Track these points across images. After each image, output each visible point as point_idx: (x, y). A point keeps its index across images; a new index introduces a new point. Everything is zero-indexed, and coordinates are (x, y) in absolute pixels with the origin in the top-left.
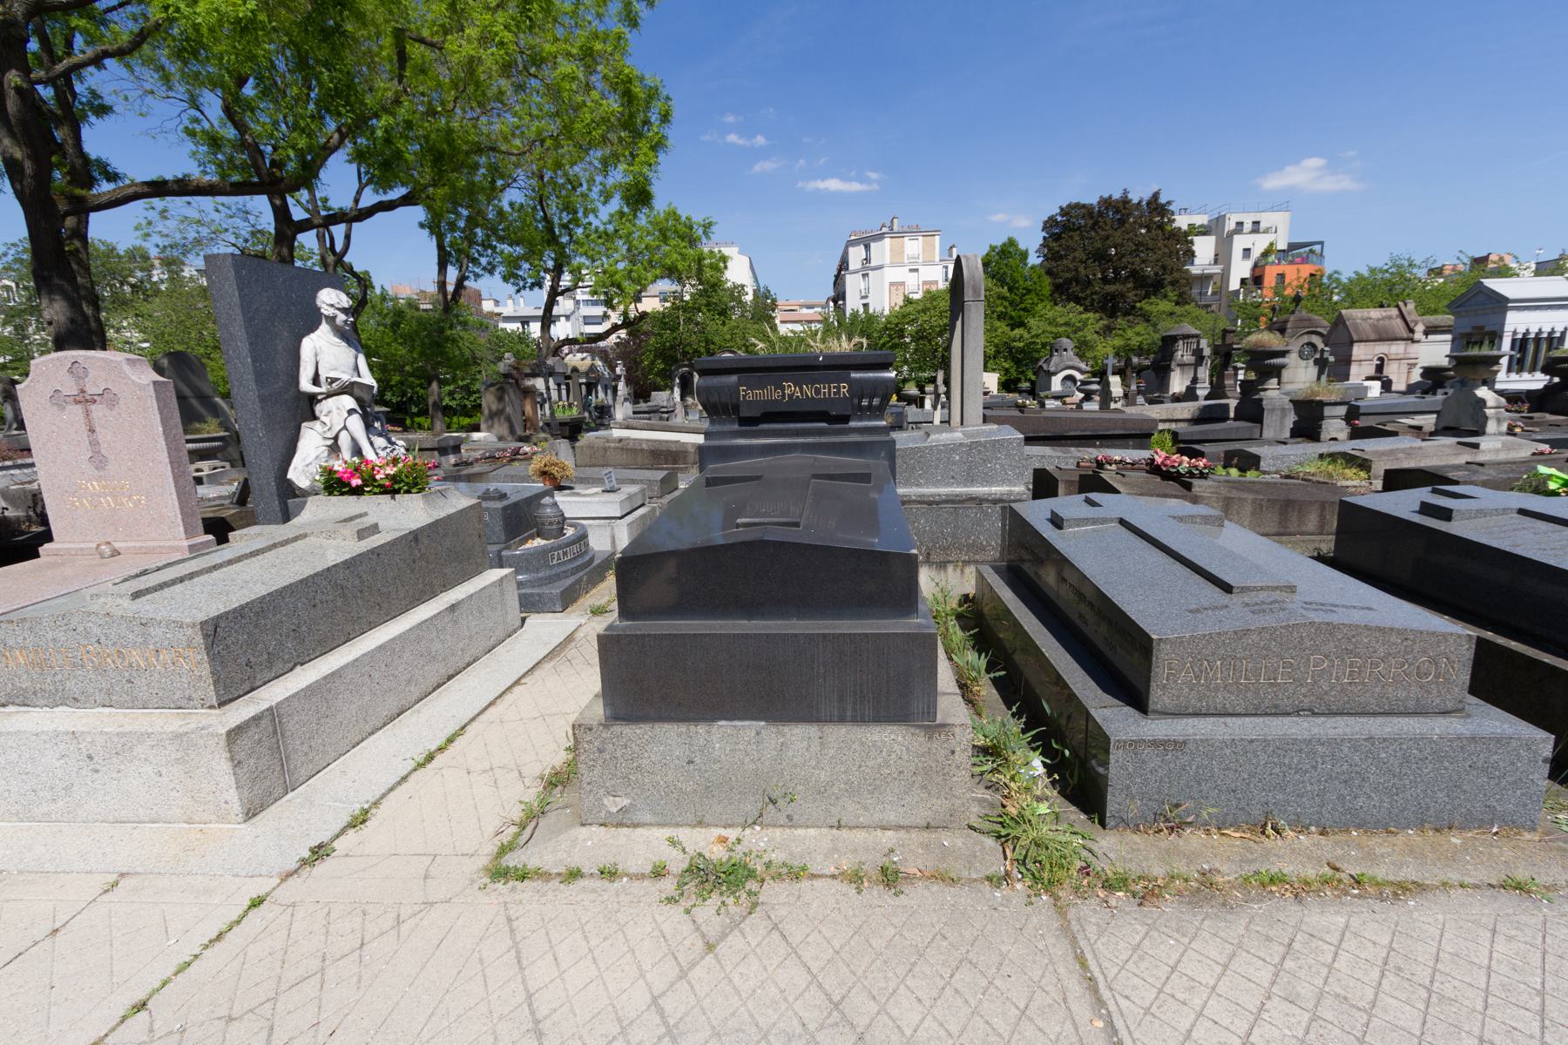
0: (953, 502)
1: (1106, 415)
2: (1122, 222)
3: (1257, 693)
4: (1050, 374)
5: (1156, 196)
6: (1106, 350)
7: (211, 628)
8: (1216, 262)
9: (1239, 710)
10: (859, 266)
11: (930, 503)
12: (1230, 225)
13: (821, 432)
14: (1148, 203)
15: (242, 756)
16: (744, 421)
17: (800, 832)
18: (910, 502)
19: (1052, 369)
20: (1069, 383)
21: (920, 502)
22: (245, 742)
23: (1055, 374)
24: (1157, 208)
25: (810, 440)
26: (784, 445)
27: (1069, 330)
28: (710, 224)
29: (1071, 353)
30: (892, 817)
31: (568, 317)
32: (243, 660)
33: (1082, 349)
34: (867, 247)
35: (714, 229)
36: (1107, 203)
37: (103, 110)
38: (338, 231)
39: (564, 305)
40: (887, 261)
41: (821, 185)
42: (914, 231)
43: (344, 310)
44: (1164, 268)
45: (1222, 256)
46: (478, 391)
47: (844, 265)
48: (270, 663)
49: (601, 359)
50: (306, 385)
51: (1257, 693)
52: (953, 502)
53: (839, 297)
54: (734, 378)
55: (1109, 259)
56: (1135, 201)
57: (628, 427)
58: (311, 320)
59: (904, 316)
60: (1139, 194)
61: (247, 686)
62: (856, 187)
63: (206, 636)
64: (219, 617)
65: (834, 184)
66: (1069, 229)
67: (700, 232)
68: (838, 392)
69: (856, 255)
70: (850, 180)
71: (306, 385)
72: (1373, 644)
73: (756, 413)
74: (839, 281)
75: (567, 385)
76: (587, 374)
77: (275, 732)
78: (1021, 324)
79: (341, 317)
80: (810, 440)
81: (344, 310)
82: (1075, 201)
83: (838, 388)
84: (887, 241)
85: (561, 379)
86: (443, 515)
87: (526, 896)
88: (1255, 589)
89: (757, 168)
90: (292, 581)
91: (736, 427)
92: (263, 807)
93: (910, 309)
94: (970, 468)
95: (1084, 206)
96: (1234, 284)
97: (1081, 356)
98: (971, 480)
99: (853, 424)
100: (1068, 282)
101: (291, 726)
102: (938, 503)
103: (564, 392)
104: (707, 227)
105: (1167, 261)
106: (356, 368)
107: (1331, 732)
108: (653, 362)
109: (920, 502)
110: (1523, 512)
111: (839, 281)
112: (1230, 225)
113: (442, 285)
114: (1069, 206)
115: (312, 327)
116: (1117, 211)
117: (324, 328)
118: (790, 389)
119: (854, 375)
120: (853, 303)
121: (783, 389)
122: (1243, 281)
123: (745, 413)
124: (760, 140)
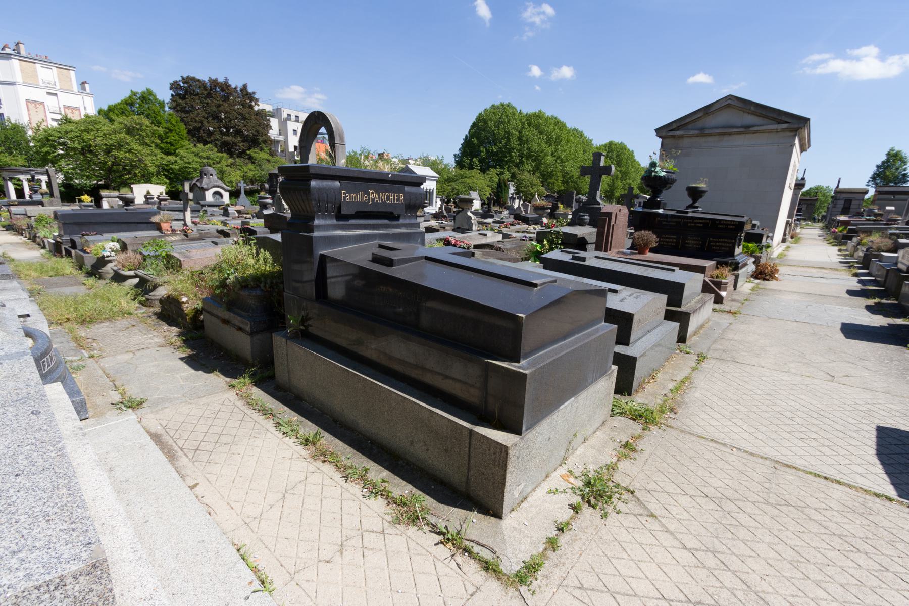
1: (98, 211)
2: (226, 99)
4: (203, 190)
5: (245, 86)
6: (235, 176)
8: (280, 134)
12: (284, 115)
14: (242, 90)
16: (340, 216)
19: (205, 187)
20: (218, 197)
23: (207, 190)
24: (247, 96)
25: (381, 231)
27: (211, 162)
29: (215, 177)
33: (222, 174)
36: (214, 83)
42: (46, 61)
44: (257, 131)
45: (283, 131)
46: (135, 175)
54: (337, 183)
55: (221, 120)
56: (233, 86)
60: (236, 83)
66: (188, 92)
73: (352, 211)
78: (173, 153)
80: (381, 231)
82: (192, 75)
91: (334, 222)
93: (69, 127)
95: (199, 81)
96: (291, 149)
97: (221, 179)
99: (402, 221)
100: (195, 128)
105: (260, 129)
110: (596, 257)
112: (284, 115)
114: (188, 77)
116: (222, 90)
119: (407, 189)
121: (368, 194)
122: (295, 148)
123: (344, 211)
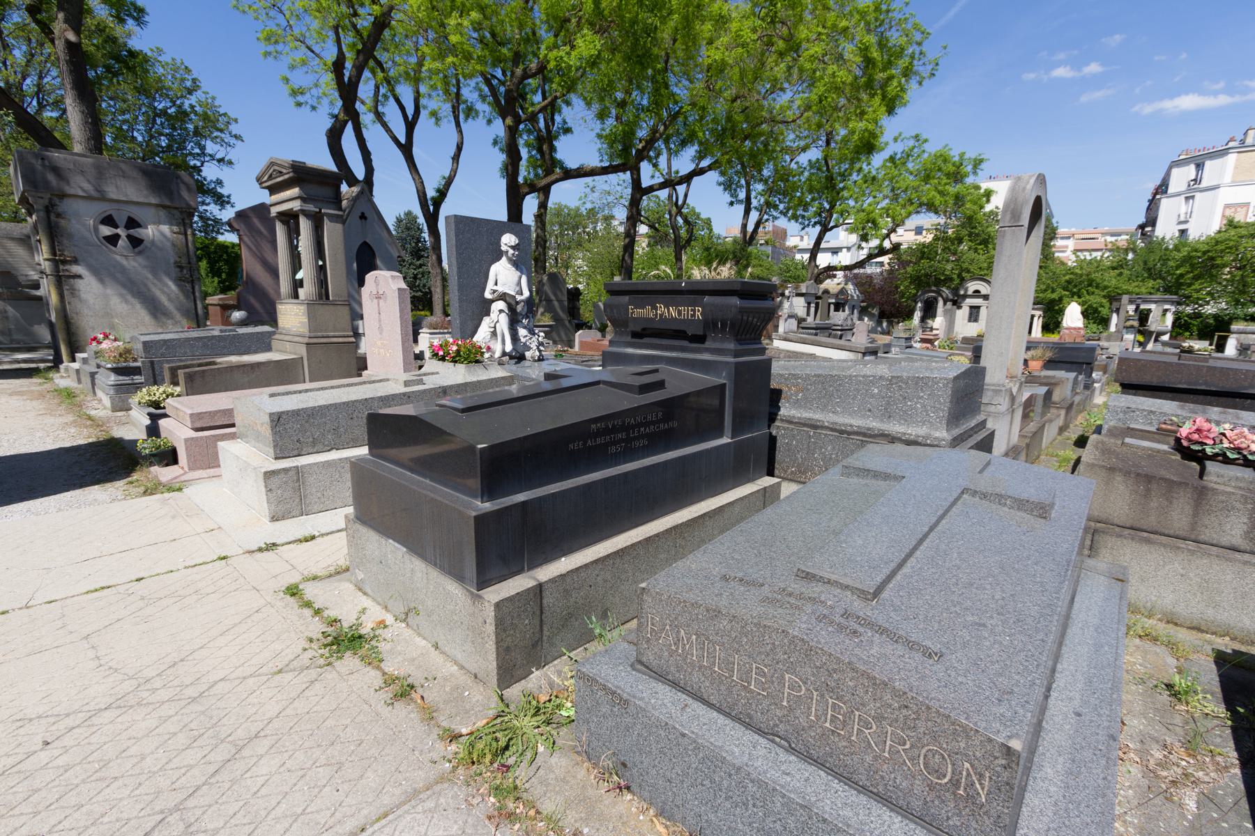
0: (864, 435)
3: (729, 690)
7: (276, 418)
9: (713, 700)
10: (1184, 187)
11: (842, 432)
13: (683, 349)
15: (273, 487)
16: (635, 335)
17: (418, 639)
18: (822, 427)
21: (832, 430)
22: (275, 481)
25: (674, 354)
26: (654, 356)
28: (981, 161)
30: (459, 657)
31: (849, 249)
32: (295, 438)
34: (1200, 166)
35: (983, 166)
37: (568, 131)
38: (681, 189)
39: (831, 240)
40: (1227, 179)
41: (1168, 105)
43: (512, 247)
47: (1162, 188)
48: (314, 443)
49: (856, 285)
50: (488, 295)
51: (729, 690)
52: (864, 435)
53: (1151, 221)
54: (626, 298)
57: (785, 340)
58: (498, 255)
59: (1217, 243)
61: (296, 452)
62: (1223, 100)
63: (272, 421)
64: (283, 412)
65: (1189, 102)
67: (969, 168)
68: (693, 315)
69: (1181, 178)
70: (1215, 94)
71: (488, 295)
72: (860, 692)
74: (1153, 206)
75: (817, 304)
76: (836, 296)
77: (298, 480)
79: (511, 251)
80: (674, 354)
81: (512, 247)
83: (694, 311)
84: (1232, 158)
85: (812, 299)
86: (475, 379)
87: (279, 604)
88: (820, 579)
89: (1084, 99)
90: (339, 401)
91: (629, 339)
92: (283, 518)
94: (888, 403)
98: (888, 416)
101: (311, 479)
102: (849, 433)
103: (813, 310)
104: (977, 163)
106: (519, 283)
107: (773, 774)
108: (907, 288)
109: (832, 430)
111: (1153, 206)
113: (744, 226)
115: (499, 259)
117: (504, 258)
118: (661, 309)
119: (707, 299)
120: (1166, 229)
124: (1094, 68)
